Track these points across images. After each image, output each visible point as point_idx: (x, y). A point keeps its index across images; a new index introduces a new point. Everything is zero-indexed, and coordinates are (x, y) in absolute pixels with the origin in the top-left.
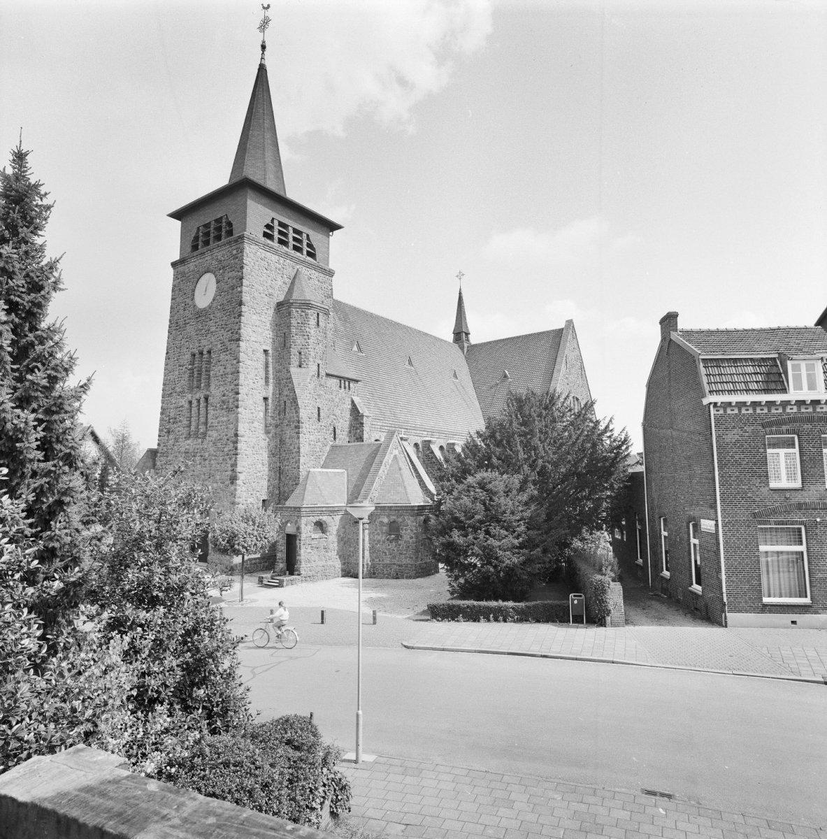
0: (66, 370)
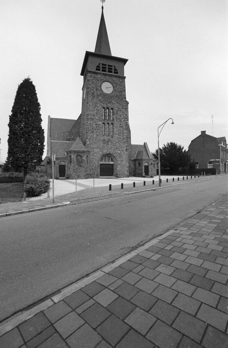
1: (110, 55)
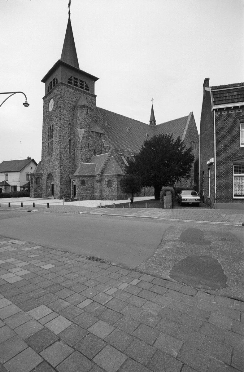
0: (211, 207)
1: (78, 69)
